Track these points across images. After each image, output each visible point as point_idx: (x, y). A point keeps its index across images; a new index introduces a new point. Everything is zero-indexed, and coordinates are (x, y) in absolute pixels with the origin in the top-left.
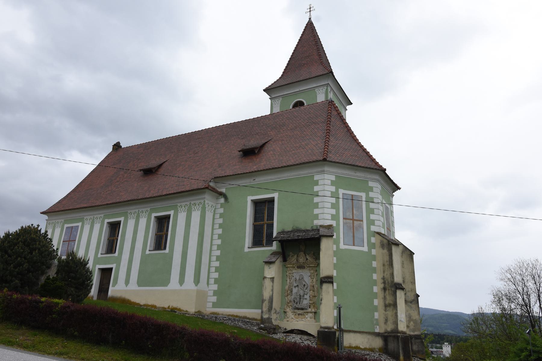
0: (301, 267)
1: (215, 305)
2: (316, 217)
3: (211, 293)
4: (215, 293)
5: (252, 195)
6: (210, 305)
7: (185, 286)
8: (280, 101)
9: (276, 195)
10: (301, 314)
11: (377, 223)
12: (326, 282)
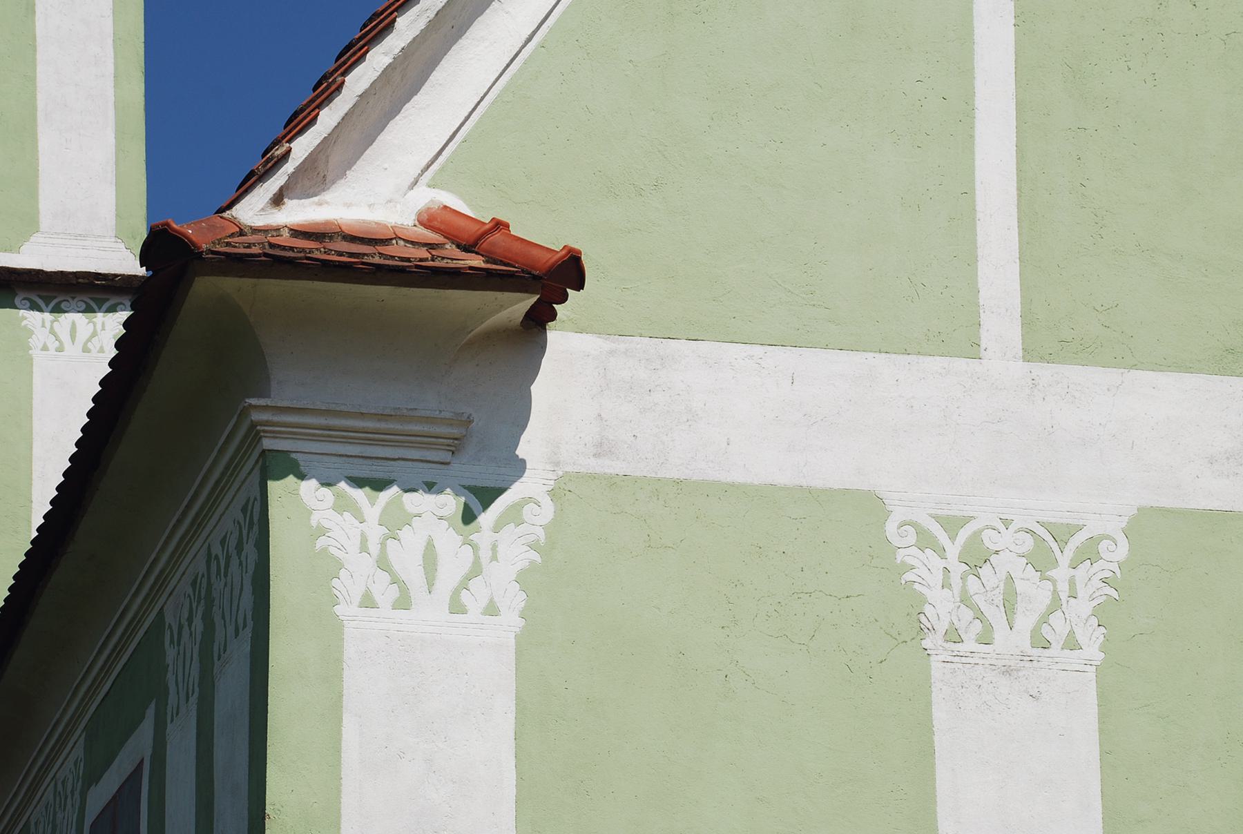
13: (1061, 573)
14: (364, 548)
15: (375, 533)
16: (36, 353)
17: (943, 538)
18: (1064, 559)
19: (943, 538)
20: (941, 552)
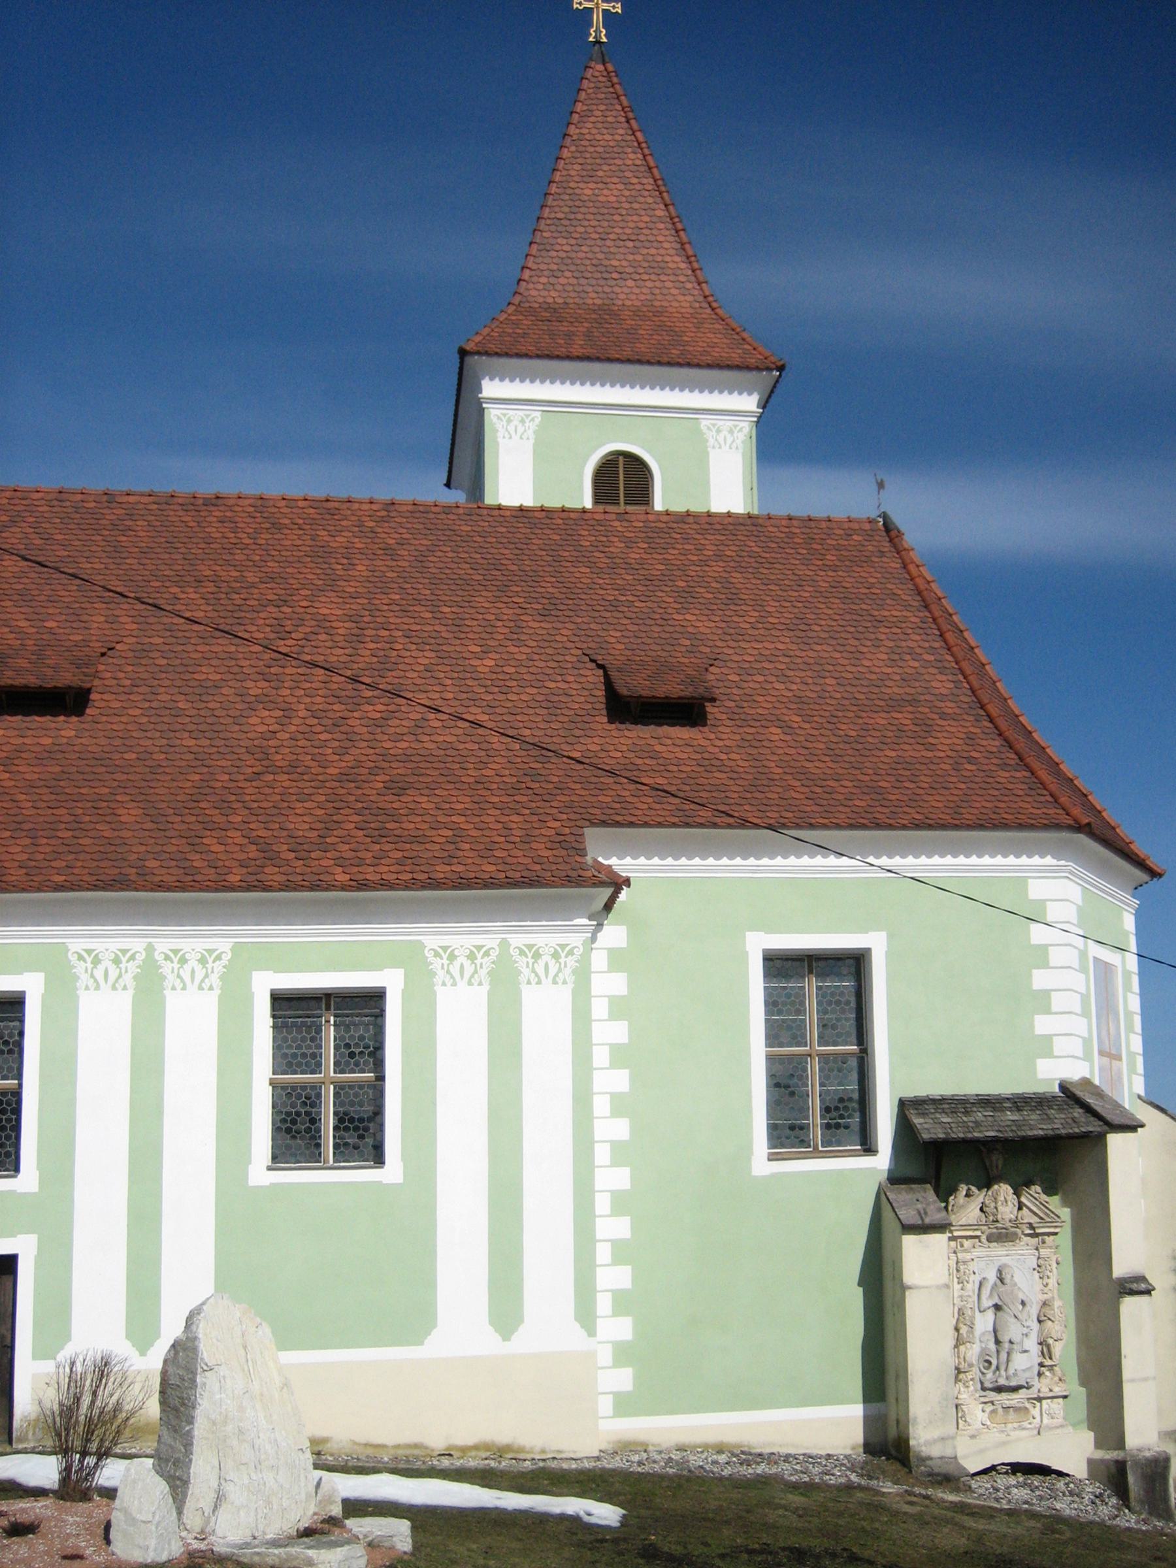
0: (1002, 1236)
1: (624, 1405)
2: (1045, 1046)
3: (605, 1356)
4: (623, 1354)
5: (770, 930)
6: (605, 1405)
7: (525, 1341)
8: (532, 427)
9: (875, 942)
10: (1017, 1409)
11: (1059, 1045)
12: (1132, 1293)
13: (209, 966)
14: (443, 968)
15: (90, 966)
16: (500, 440)
17: (172, 955)
18: (563, 955)
19: (172, 955)
20: (85, 961)
